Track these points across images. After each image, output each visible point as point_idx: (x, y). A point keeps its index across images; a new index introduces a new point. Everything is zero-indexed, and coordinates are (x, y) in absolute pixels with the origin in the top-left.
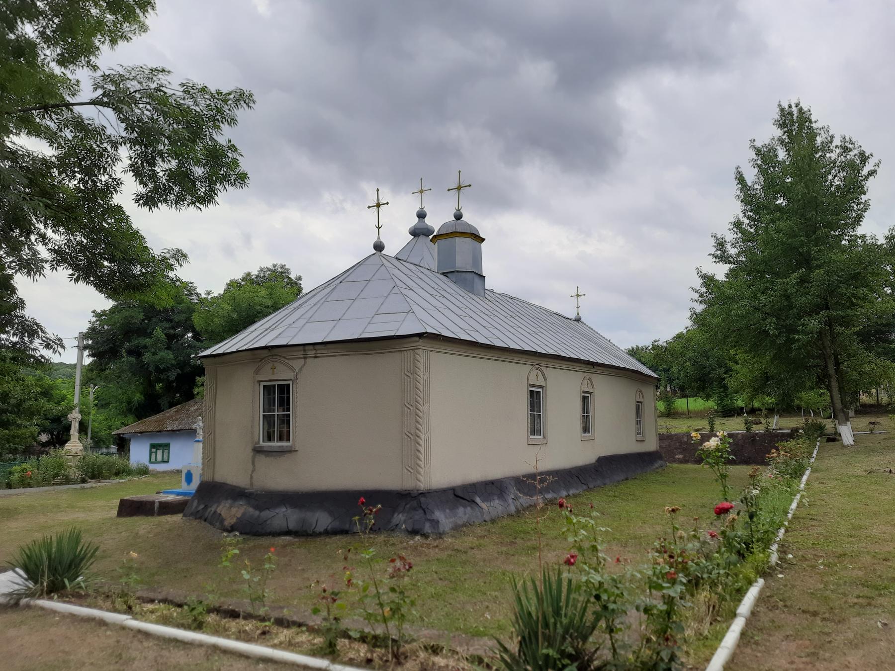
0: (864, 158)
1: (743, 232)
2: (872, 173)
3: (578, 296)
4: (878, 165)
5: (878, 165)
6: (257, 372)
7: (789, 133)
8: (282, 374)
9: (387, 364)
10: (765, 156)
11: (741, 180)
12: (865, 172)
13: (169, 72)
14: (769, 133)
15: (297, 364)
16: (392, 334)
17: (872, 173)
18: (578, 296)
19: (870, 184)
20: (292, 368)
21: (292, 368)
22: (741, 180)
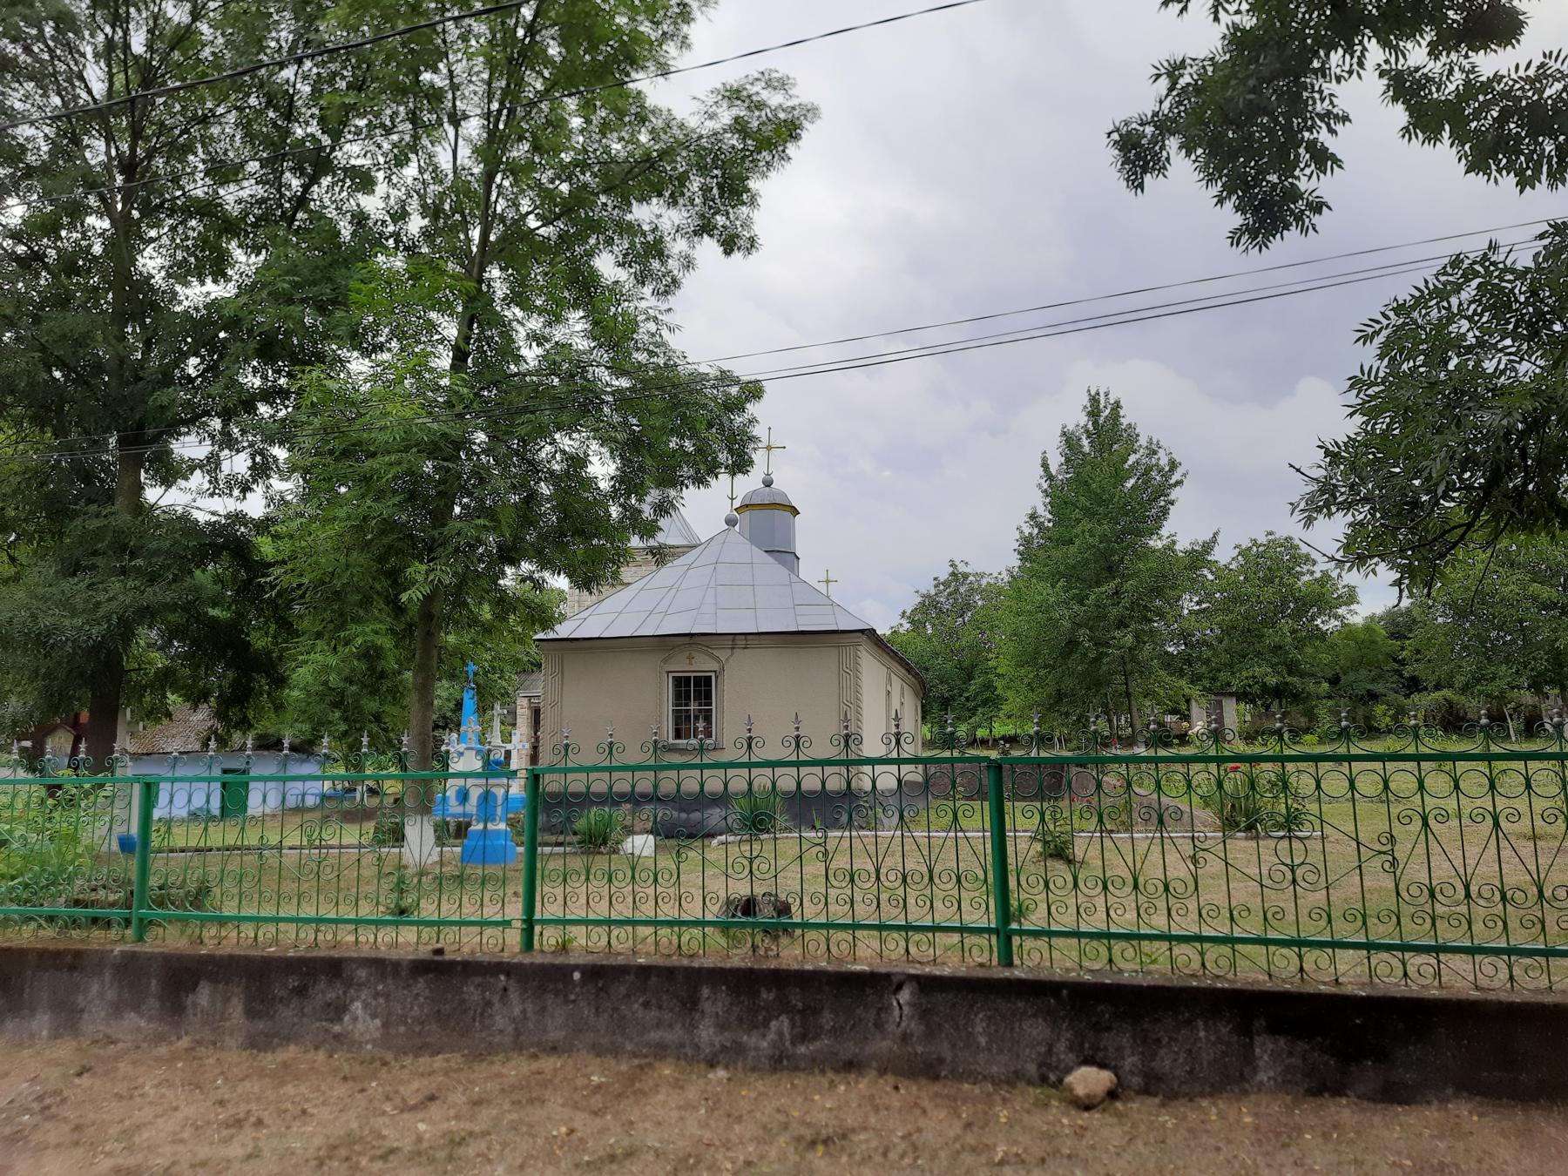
0: (1173, 465)
1: (1040, 526)
2: (1179, 483)
3: (827, 582)
4: (1184, 475)
5: (1184, 475)
6: (665, 661)
7: (1095, 423)
8: (702, 664)
9: (823, 662)
10: (1070, 440)
11: (1045, 466)
12: (1172, 481)
13: (1215, 535)
14: (1077, 418)
15: (723, 655)
16: (834, 628)
17: (1179, 483)
18: (827, 582)
19: (1175, 494)
20: (717, 659)
21: (717, 659)
22: (1045, 466)
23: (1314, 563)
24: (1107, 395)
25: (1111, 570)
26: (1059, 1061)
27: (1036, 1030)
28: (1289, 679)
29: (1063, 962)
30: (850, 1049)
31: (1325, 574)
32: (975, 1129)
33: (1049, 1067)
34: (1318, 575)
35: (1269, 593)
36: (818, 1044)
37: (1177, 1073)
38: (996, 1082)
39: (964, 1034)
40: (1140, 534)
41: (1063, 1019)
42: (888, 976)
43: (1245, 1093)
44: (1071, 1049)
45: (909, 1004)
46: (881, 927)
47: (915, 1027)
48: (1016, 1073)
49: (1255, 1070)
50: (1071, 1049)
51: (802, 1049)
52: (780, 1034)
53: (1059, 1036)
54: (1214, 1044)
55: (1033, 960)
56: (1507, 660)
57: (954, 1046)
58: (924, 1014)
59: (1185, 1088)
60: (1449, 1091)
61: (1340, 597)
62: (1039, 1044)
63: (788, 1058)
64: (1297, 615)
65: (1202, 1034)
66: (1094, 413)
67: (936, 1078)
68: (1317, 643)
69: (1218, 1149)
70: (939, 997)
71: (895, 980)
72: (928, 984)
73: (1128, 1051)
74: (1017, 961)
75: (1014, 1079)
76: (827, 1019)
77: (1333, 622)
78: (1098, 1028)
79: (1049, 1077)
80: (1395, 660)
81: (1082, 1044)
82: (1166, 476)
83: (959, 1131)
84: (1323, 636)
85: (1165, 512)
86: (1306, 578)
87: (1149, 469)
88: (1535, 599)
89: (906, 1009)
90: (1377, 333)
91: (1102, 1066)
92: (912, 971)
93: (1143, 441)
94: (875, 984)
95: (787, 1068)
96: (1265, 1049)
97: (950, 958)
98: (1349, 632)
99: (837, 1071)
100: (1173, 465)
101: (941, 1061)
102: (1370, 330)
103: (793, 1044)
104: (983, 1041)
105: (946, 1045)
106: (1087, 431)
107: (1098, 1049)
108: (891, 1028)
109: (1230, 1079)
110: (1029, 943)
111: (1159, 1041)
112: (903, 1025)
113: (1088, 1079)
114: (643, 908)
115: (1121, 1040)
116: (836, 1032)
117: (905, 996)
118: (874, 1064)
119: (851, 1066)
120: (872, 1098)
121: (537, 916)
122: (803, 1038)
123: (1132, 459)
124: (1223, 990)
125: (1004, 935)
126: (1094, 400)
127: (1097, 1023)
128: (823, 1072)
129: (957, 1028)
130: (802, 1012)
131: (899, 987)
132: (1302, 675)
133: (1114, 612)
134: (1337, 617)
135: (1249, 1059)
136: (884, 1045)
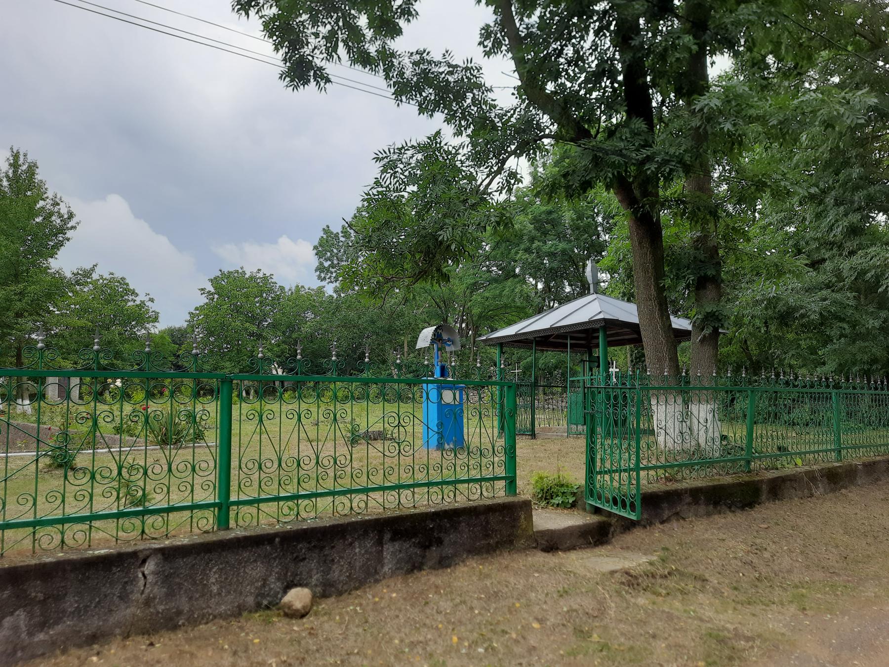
2: (73, 228)
4: (78, 223)
12: (69, 226)
17: (73, 228)
19: (69, 234)
23: (137, 295)
24: (25, 155)
25: (17, 277)
26: (271, 589)
27: (256, 571)
28: (115, 362)
29: (267, 519)
30: (94, 623)
31: (143, 302)
32: (240, 654)
33: (263, 596)
34: (138, 302)
35: (108, 310)
36: (59, 628)
37: (342, 578)
38: (225, 617)
39: (200, 587)
40: (40, 254)
41: (275, 559)
42: (134, 554)
43: (377, 581)
44: (278, 579)
45: (153, 573)
46: (429, 484)
47: (159, 591)
48: (239, 607)
49: (382, 566)
50: (278, 579)
51: (41, 636)
52: (15, 628)
53: (272, 571)
54: (363, 555)
55: (247, 522)
56: (230, 360)
57: (191, 598)
58: (166, 578)
59: (345, 587)
60: (465, 556)
61: (150, 317)
62: (257, 581)
63: (23, 649)
64: (124, 324)
65: (357, 550)
66: (15, 165)
67: (175, 628)
68: (134, 342)
69: (397, 616)
70: (180, 562)
71: (141, 556)
72: (170, 554)
73: (315, 571)
74: (232, 524)
75: (239, 612)
76: (70, 603)
77: (143, 331)
78: (298, 560)
79: (268, 604)
80: (174, 355)
81: (286, 574)
82: (65, 221)
83: (231, 659)
84: (137, 338)
85: (60, 244)
86: (130, 304)
87: (51, 214)
88: (246, 329)
89: (150, 578)
90: (383, 158)
91: (301, 585)
92: (157, 546)
93: (50, 194)
94: (120, 563)
95: (21, 659)
96: (390, 550)
97: (184, 531)
98: (149, 336)
99: (80, 646)
100: (71, 216)
101: (179, 613)
102: (381, 156)
103: (31, 634)
104: (215, 589)
105: (184, 599)
106: (7, 176)
107: (297, 575)
108: (136, 596)
109: (368, 576)
110: (245, 509)
111: (333, 560)
112: (147, 591)
113: (298, 597)
114: (247, 490)
115: (312, 567)
116: (78, 613)
117: (150, 567)
118: (118, 631)
119: (95, 639)
120: (299, 642)
121: (233, 498)
122: (43, 626)
123: (41, 203)
124: (370, 521)
125: (223, 507)
126: (16, 156)
127: (297, 557)
128: (64, 652)
129: (194, 583)
130: (43, 602)
131: (144, 561)
132: (123, 360)
133: (18, 305)
134: (145, 328)
135: (380, 561)
136: (128, 612)
